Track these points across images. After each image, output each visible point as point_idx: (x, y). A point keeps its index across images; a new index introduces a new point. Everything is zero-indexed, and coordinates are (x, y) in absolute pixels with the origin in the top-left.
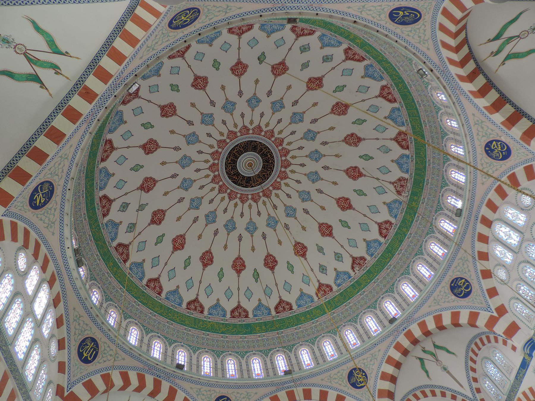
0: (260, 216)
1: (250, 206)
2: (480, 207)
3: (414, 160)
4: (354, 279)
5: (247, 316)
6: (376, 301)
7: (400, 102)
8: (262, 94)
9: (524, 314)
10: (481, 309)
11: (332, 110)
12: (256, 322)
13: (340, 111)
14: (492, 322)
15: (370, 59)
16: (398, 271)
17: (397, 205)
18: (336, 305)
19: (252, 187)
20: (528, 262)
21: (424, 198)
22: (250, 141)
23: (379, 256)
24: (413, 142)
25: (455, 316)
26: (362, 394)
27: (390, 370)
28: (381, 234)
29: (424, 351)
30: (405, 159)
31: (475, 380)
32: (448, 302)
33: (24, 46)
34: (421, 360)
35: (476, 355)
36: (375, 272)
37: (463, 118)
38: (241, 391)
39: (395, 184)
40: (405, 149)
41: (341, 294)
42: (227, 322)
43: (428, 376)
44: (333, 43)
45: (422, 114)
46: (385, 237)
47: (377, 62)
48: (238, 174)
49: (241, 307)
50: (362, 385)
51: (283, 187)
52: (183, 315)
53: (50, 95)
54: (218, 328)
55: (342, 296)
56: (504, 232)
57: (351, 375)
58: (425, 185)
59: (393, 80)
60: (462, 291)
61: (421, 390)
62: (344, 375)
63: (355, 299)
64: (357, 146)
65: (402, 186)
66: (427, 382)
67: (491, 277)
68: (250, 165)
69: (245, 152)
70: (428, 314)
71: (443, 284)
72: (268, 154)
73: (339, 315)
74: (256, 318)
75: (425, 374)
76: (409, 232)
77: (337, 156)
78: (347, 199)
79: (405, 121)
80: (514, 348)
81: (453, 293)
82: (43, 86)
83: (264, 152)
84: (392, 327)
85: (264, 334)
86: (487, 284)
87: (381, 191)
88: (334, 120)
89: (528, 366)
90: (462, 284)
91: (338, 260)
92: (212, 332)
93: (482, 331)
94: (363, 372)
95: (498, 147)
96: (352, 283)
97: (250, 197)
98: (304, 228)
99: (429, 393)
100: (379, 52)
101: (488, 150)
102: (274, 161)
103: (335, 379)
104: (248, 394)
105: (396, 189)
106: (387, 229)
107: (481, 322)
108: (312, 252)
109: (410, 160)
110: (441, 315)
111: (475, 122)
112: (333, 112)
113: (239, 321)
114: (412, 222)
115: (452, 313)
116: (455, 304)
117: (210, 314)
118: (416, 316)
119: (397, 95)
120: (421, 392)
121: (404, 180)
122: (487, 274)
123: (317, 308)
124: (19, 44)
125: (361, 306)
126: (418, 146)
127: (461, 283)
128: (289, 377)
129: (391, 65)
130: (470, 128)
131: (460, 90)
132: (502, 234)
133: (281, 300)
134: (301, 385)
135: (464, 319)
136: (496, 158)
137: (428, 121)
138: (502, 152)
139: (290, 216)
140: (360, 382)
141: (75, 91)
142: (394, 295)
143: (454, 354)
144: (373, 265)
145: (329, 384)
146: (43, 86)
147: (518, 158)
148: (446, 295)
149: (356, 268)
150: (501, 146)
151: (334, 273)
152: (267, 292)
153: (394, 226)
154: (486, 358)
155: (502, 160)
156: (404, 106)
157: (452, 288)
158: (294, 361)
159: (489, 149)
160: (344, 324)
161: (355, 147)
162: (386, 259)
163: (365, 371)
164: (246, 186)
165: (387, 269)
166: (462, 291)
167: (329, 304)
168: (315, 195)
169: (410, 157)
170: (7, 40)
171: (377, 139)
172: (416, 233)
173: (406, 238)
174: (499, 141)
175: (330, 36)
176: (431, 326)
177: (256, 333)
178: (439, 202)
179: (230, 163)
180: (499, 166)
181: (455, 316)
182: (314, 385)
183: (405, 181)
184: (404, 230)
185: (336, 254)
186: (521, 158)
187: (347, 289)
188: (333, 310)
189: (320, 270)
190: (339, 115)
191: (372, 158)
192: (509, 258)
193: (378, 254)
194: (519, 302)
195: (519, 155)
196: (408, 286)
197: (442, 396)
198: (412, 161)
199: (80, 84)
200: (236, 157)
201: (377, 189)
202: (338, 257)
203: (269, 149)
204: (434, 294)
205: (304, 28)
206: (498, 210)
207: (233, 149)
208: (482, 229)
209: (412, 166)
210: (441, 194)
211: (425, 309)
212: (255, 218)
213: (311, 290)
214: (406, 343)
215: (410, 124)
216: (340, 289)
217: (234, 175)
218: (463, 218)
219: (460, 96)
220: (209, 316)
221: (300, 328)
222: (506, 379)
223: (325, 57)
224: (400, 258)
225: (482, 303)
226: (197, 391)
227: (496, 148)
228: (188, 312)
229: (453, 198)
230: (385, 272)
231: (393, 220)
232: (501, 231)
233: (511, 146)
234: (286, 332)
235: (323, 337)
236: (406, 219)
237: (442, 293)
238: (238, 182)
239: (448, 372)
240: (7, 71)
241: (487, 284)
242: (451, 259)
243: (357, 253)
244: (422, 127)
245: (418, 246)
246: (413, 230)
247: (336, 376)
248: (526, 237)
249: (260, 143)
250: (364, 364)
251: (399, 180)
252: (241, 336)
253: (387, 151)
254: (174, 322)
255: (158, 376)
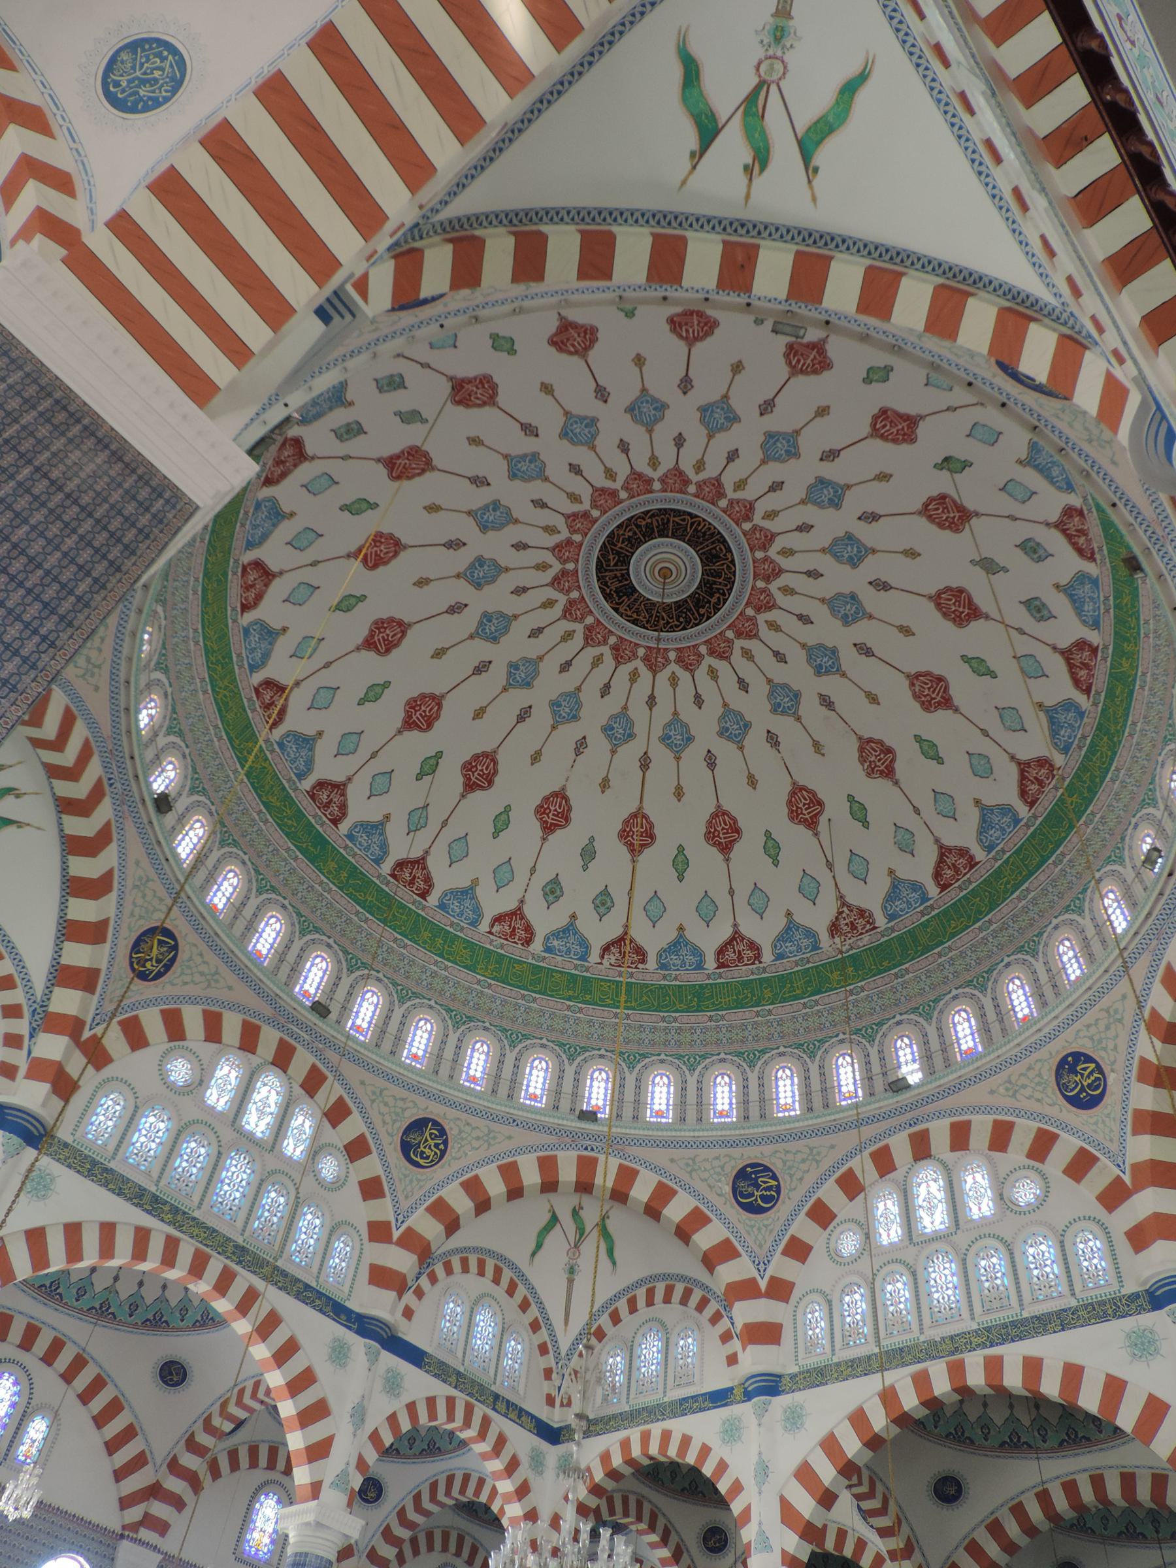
0: (561, 672)
1: (568, 636)
2: (940, 1115)
3: (926, 917)
4: (587, 970)
5: (335, 822)
6: (585, 1049)
7: (1035, 817)
8: (812, 443)
9: (810, 1332)
10: (751, 1253)
11: (918, 675)
12: (341, 850)
13: (926, 692)
14: (745, 1290)
15: (1095, 704)
16: (679, 1044)
17: (805, 942)
18: (507, 976)
19: (616, 610)
20: (914, 1274)
21: (862, 989)
22: (722, 536)
23: (674, 983)
24: (965, 892)
25: (697, 1219)
26: (406, 1176)
27: (495, 1186)
28: (721, 952)
29: (575, 1213)
30: (916, 895)
31: (600, 1335)
32: (710, 1186)
33: (784, 74)
34: (554, 1219)
35: (650, 1303)
36: (636, 1000)
37: (1103, 980)
38: (210, 956)
39: (845, 909)
40: (938, 884)
41: (536, 969)
42: (293, 795)
43: (534, 1254)
44: (1086, 608)
45: (1040, 878)
46: (721, 965)
47: (1099, 723)
48: (625, 560)
49: (343, 794)
50: (422, 1162)
51: (663, 676)
52: (236, 695)
53: (684, 183)
54: (267, 788)
55: (534, 974)
56: (929, 1193)
57: (419, 1125)
58: (893, 972)
59: (1077, 776)
60: (753, 1195)
61: (499, 1264)
62: (408, 1114)
63: (552, 1004)
64: (869, 775)
65: (853, 926)
66: (522, 1261)
67: (825, 1227)
68: (665, 573)
69: (689, 543)
70: (655, 1169)
71: (736, 1152)
72: (717, 595)
73: (493, 999)
74: (348, 842)
75: (533, 1246)
76: (771, 1007)
77: (817, 746)
78: (738, 831)
79: (998, 848)
80: (732, 1360)
81: (734, 1183)
82: (697, 156)
83: (715, 583)
84: (573, 1124)
85: (334, 888)
86: (803, 1228)
87: (809, 889)
88: (898, 693)
89: (725, 1405)
90: (764, 1186)
91: (596, 907)
92: (252, 784)
93: (712, 1286)
94: (446, 1143)
95: (1088, 1077)
96: (577, 972)
97: (589, 620)
98: (605, 784)
99: (505, 1282)
100: (1126, 721)
101: (1068, 1063)
102: (709, 618)
103: (386, 1104)
104: (217, 973)
105: (837, 918)
106: (740, 958)
107: (729, 1272)
108: (568, 839)
109: (922, 908)
110: (674, 1193)
111: (1109, 1008)
112: (914, 678)
113: (314, 816)
114: (797, 998)
115: (697, 1208)
116: (718, 1202)
117: (281, 745)
118: (633, 1151)
119: (1047, 802)
120: (525, 1299)
121: (868, 922)
122: (822, 1215)
123: (470, 945)
124: (783, 62)
125: (551, 1029)
126: (963, 907)
127: (765, 1182)
128: (313, 1018)
129: (1112, 760)
130: (1092, 1003)
131: (1160, 947)
132: (923, 1190)
133: (423, 859)
134: (316, 1053)
135: (705, 1239)
136: (1062, 1087)
137: (1034, 899)
138: (1083, 1090)
139: (609, 737)
140: (423, 1153)
141: (724, 229)
142: (627, 1074)
143: (614, 1263)
144: (647, 986)
145: (367, 1104)
146: (697, 156)
147: (1094, 1127)
148: (719, 1174)
149: (612, 956)
150: (1094, 1081)
151: (563, 921)
152: (417, 820)
153: (758, 969)
154: (663, 1325)
155: (1068, 1099)
156: (1032, 829)
157: (742, 1175)
158: (341, 994)
159: (1071, 1063)
160: (487, 1025)
161: (863, 774)
162: (681, 1002)
163: (450, 1145)
164: (607, 597)
165: (663, 1019)
166: (753, 1195)
167: (497, 962)
168: (694, 756)
169: (928, 904)
170: (782, 37)
171: (917, 811)
172: (780, 1022)
173: (755, 1009)
174: (1101, 1071)
175: (1102, 599)
176: (641, 1191)
177: (320, 870)
178: (880, 1024)
179: (638, 526)
180: (1050, 1102)
181: (697, 1219)
182: (339, 1077)
183: (868, 927)
184: (768, 994)
185: (605, 892)
186: (1095, 1132)
187: (557, 971)
188: (493, 979)
189: (545, 887)
190: (916, 696)
191: (866, 824)
192: (890, 1233)
193: (676, 979)
194: (825, 1307)
195: (1100, 1125)
196: (669, 1086)
197: (520, 1306)
198: (923, 914)
199: (748, 232)
200: (663, 530)
201: (806, 880)
202: (603, 902)
203: (731, 589)
204: (703, 1150)
205: (1091, 535)
206: (963, 1153)
207: (678, 513)
208: (900, 1146)
209: (911, 919)
210: (898, 1018)
211: (660, 1157)
212: (549, 667)
213: (494, 903)
214: (568, 1173)
215: (1000, 862)
216: (544, 958)
217: (618, 553)
218: (895, 1100)
219: (1147, 952)
220: (276, 746)
221: (405, 947)
222: (661, 1387)
223: (1037, 603)
224: (704, 1027)
225: (761, 1246)
226: (140, 879)
227: (1082, 1075)
228: (250, 700)
229: (911, 1048)
230: (654, 1019)
231: (767, 956)
232: (928, 1186)
233: (1107, 1100)
234: (374, 926)
235: (431, 1007)
236: (791, 983)
237: (716, 1163)
238: (606, 571)
239: (571, 1281)
240: (697, 66)
241: (803, 1228)
242: (791, 1134)
243: (642, 933)
244: (1012, 893)
245: (761, 1045)
246: (781, 1010)
247: (391, 1101)
248: (955, 1238)
249: (733, 562)
250: (461, 1132)
251: (862, 913)
252: (292, 847)
253: (906, 847)
254: (213, 690)
255: (110, 779)
